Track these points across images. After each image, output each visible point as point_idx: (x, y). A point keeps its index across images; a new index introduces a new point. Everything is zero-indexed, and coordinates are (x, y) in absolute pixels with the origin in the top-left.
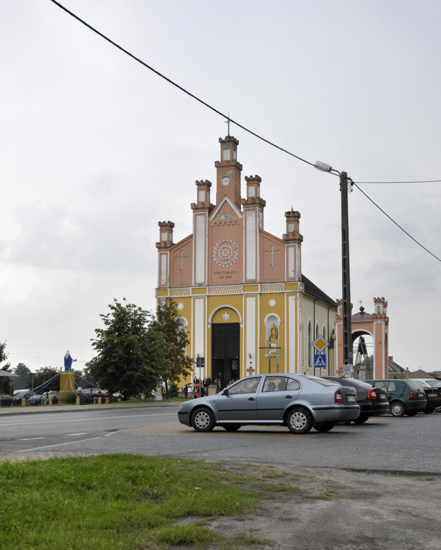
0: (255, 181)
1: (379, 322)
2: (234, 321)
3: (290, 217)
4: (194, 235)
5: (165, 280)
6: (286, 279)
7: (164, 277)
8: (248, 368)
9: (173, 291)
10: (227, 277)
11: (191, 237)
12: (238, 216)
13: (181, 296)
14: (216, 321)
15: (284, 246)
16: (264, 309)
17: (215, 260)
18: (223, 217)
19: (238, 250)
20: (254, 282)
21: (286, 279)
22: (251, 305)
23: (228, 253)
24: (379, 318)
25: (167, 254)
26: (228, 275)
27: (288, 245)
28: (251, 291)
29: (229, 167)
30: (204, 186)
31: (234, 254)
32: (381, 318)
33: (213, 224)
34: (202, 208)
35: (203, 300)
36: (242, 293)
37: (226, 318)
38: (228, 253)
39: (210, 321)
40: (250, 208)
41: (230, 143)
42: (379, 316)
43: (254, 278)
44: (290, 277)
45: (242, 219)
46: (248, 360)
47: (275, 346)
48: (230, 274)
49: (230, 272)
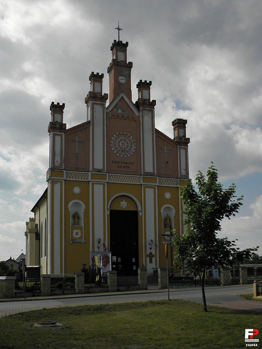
0: (144, 86)
2: (133, 209)
3: (181, 123)
4: (91, 122)
5: (59, 162)
6: (179, 176)
7: (58, 158)
8: (148, 253)
9: (69, 174)
10: (125, 167)
11: (88, 123)
12: (135, 114)
13: (77, 180)
14: (116, 208)
15: (177, 147)
16: (161, 201)
17: (113, 149)
18: (120, 111)
19: (135, 144)
20: (152, 174)
21: (179, 176)
22: (150, 194)
23: (126, 145)
25: (61, 136)
26: (126, 165)
27: (180, 146)
28: (153, 183)
29: (121, 67)
30: (96, 78)
31: (131, 147)
33: (110, 115)
34: (95, 98)
35: (102, 186)
36: (142, 182)
37: (124, 205)
38: (126, 145)
39: (109, 207)
40: (147, 109)
41: (119, 47)
43: (152, 171)
44: (182, 174)
45: (139, 117)
46: (148, 246)
47: (166, 237)
48: (128, 165)
49: (128, 163)
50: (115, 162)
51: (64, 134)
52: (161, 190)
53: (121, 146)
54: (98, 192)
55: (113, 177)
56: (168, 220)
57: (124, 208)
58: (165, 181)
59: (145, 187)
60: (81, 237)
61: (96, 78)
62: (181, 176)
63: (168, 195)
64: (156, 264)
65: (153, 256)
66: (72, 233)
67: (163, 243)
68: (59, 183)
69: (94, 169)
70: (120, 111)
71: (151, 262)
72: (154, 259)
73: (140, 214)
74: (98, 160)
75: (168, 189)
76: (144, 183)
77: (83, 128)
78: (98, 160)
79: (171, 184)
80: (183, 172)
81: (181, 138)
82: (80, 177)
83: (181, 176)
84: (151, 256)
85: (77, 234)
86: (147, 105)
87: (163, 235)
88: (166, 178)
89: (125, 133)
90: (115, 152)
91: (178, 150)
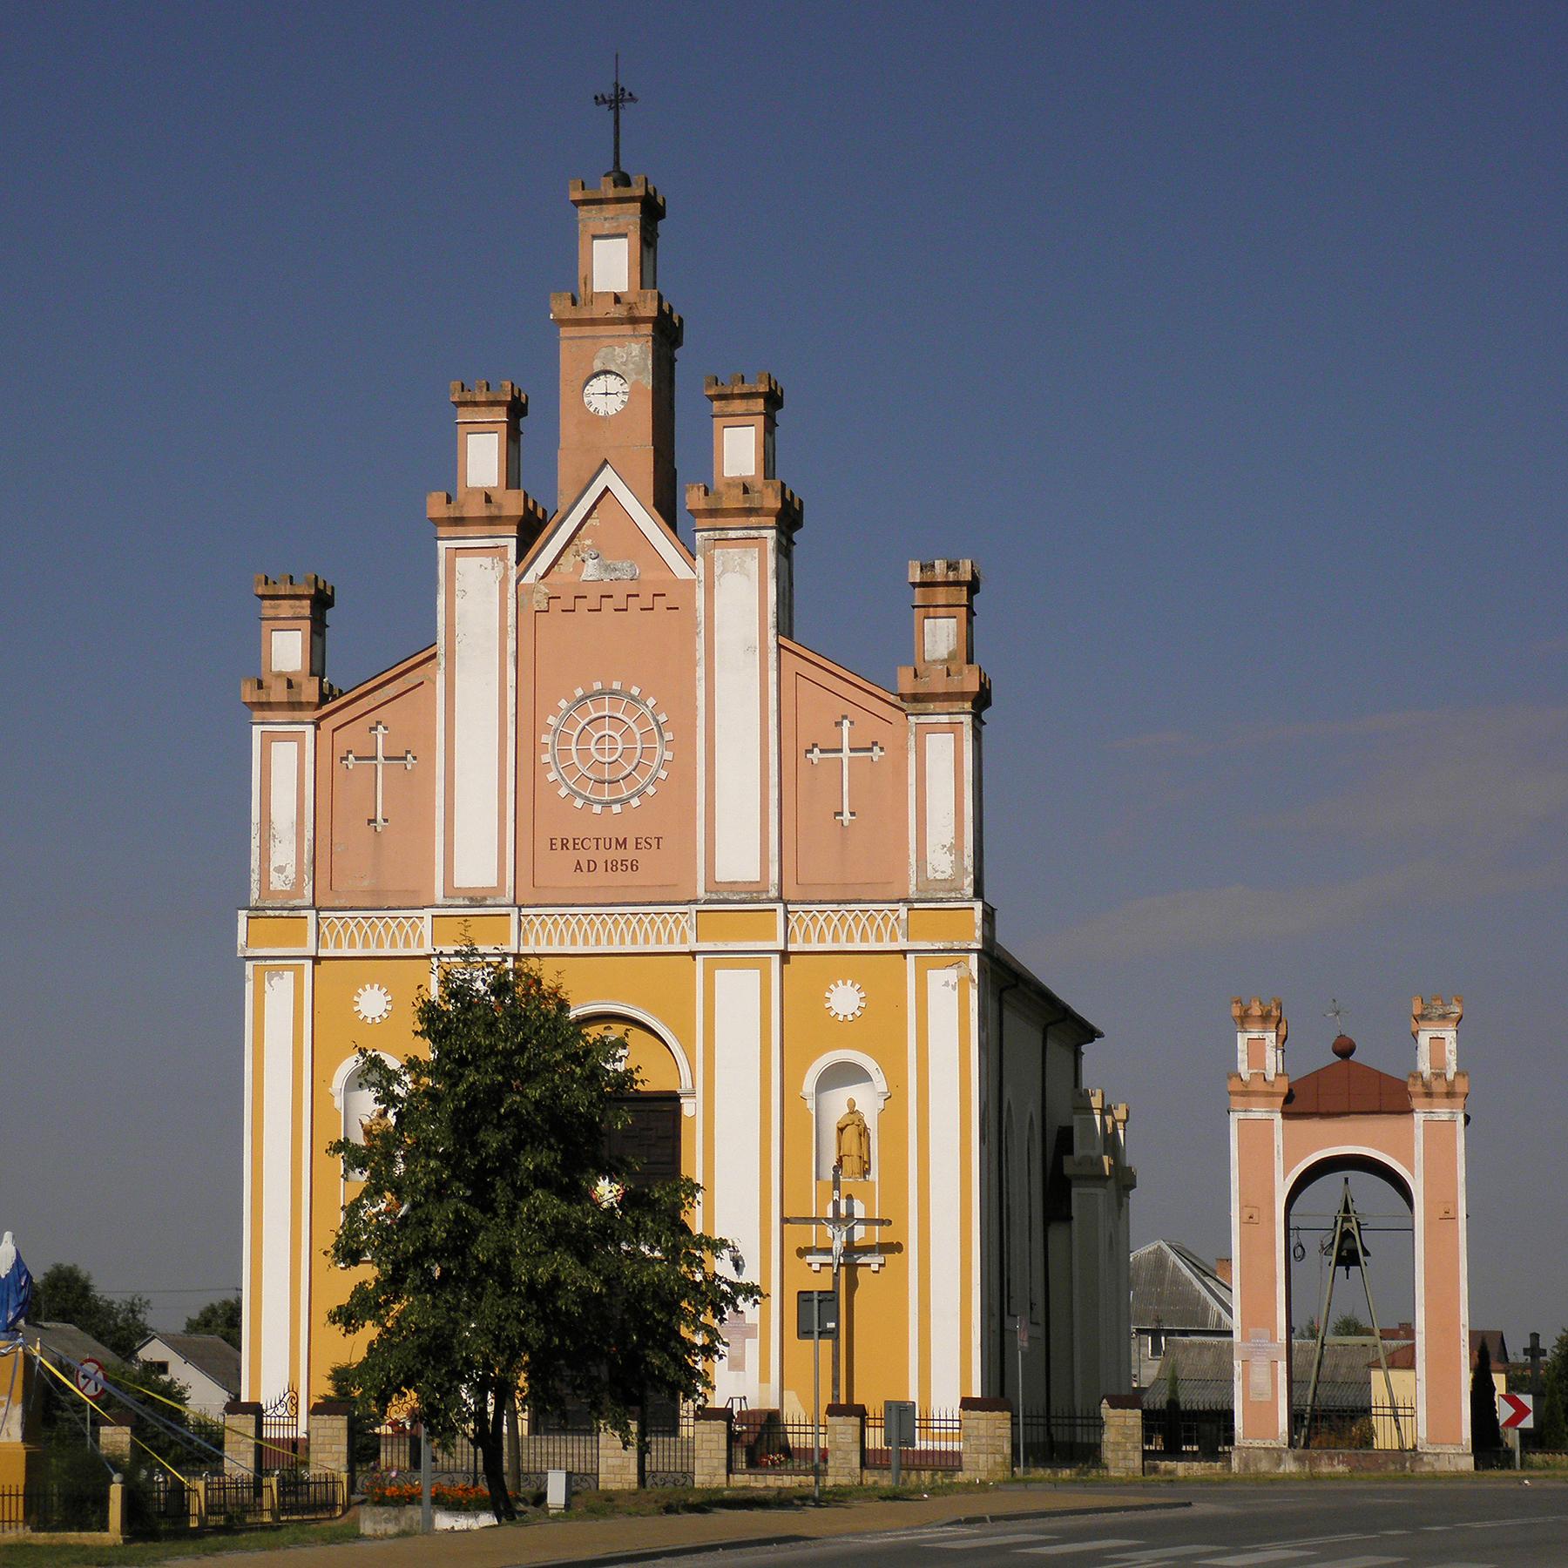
1: (1443, 1114)
5: (291, 871)
10: (612, 866)
15: (906, 727)
20: (751, 894)
24: (1440, 1095)
32: (1450, 1094)
42: (1438, 1086)
48: (630, 853)
49: (631, 843)
50: (564, 845)
64: (764, 1377)
88: (834, 907)
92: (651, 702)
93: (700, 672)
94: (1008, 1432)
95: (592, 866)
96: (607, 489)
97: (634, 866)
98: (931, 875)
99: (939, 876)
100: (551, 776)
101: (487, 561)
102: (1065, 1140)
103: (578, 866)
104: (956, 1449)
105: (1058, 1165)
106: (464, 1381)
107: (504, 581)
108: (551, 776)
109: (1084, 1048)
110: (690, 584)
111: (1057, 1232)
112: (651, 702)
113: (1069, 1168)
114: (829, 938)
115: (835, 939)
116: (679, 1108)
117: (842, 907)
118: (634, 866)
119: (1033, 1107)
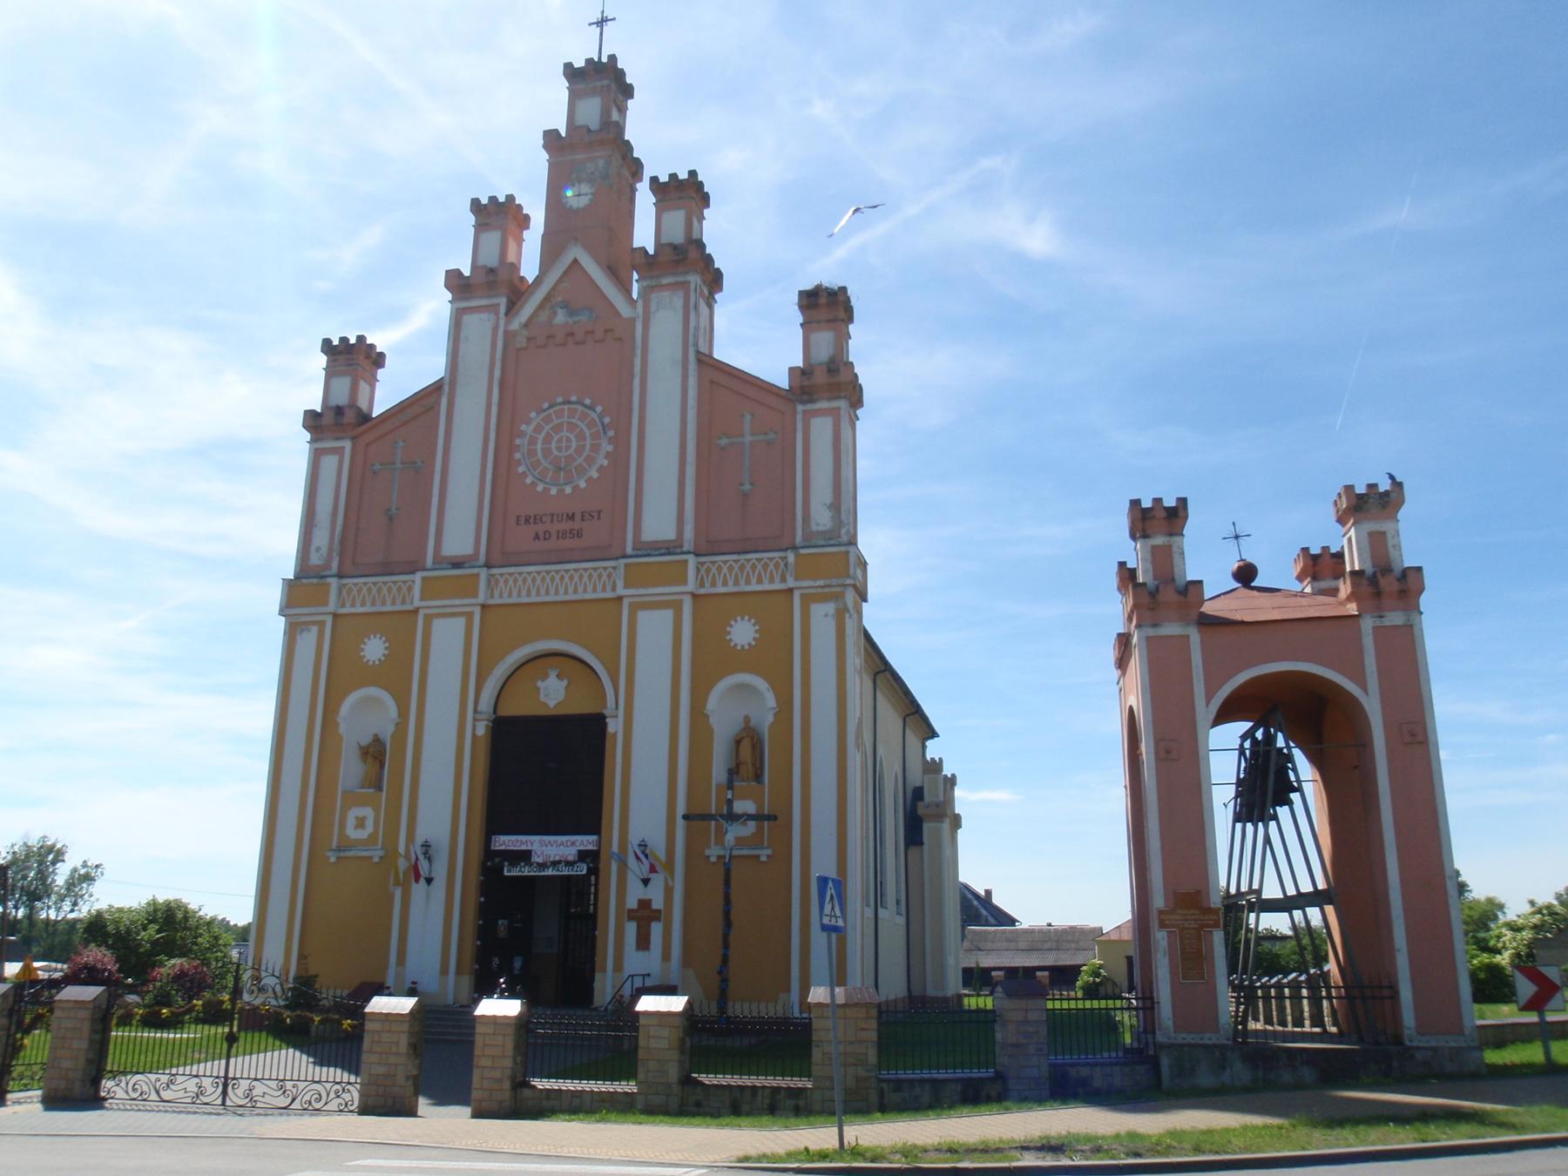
0: (686, 194)
5: (324, 550)
7: (321, 538)
8: (632, 903)
10: (562, 535)
11: (436, 388)
14: (516, 707)
15: (794, 413)
16: (709, 661)
20: (669, 548)
23: (574, 444)
27: (809, 407)
30: (497, 216)
33: (521, 342)
45: (633, 320)
48: (576, 525)
49: (578, 517)
50: (527, 521)
51: (347, 445)
52: (711, 613)
53: (555, 452)
54: (448, 643)
55: (506, 582)
56: (746, 747)
57: (552, 704)
58: (731, 569)
59: (635, 608)
60: (372, 838)
61: (497, 216)
62: (808, 535)
63: (743, 633)
64: (666, 956)
65: (656, 915)
66: (343, 825)
67: (707, 852)
68: (315, 629)
69: (440, 561)
70: (561, 317)
71: (643, 942)
72: (656, 929)
73: (611, 728)
74: (460, 526)
75: (743, 602)
76: (799, 584)
77: (425, 405)
78: (460, 526)
79: (760, 581)
80: (822, 518)
81: (339, 411)
82: (756, 574)
83: (808, 535)
84: (645, 915)
85: (360, 823)
86: (689, 267)
87: (772, 818)
88: (735, 557)
89: (588, 401)
90: (529, 480)
91: (799, 425)
92: (599, 409)
93: (637, 382)
94: (666, 294)
95: (547, 535)
96: (575, 261)
97: (579, 534)
98: (814, 528)
99: (821, 528)
100: (521, 469)
101: (484, 316)
102: (918, 793)
103: (537, 537)
104: (990, 1006)
105: (914, 808)
106: (1127, 1050)
107: (495, 329)
108: (521, 469)
109: (928, 743)
110: (633, 320)
111: (913, 851)
112: (599, 409)
113: (921, 811)
114: (731, 583)
115: (736, 583)
116: (605, 725)
117: (743, 557)
118: (579, 534)
119: (898, 768)
